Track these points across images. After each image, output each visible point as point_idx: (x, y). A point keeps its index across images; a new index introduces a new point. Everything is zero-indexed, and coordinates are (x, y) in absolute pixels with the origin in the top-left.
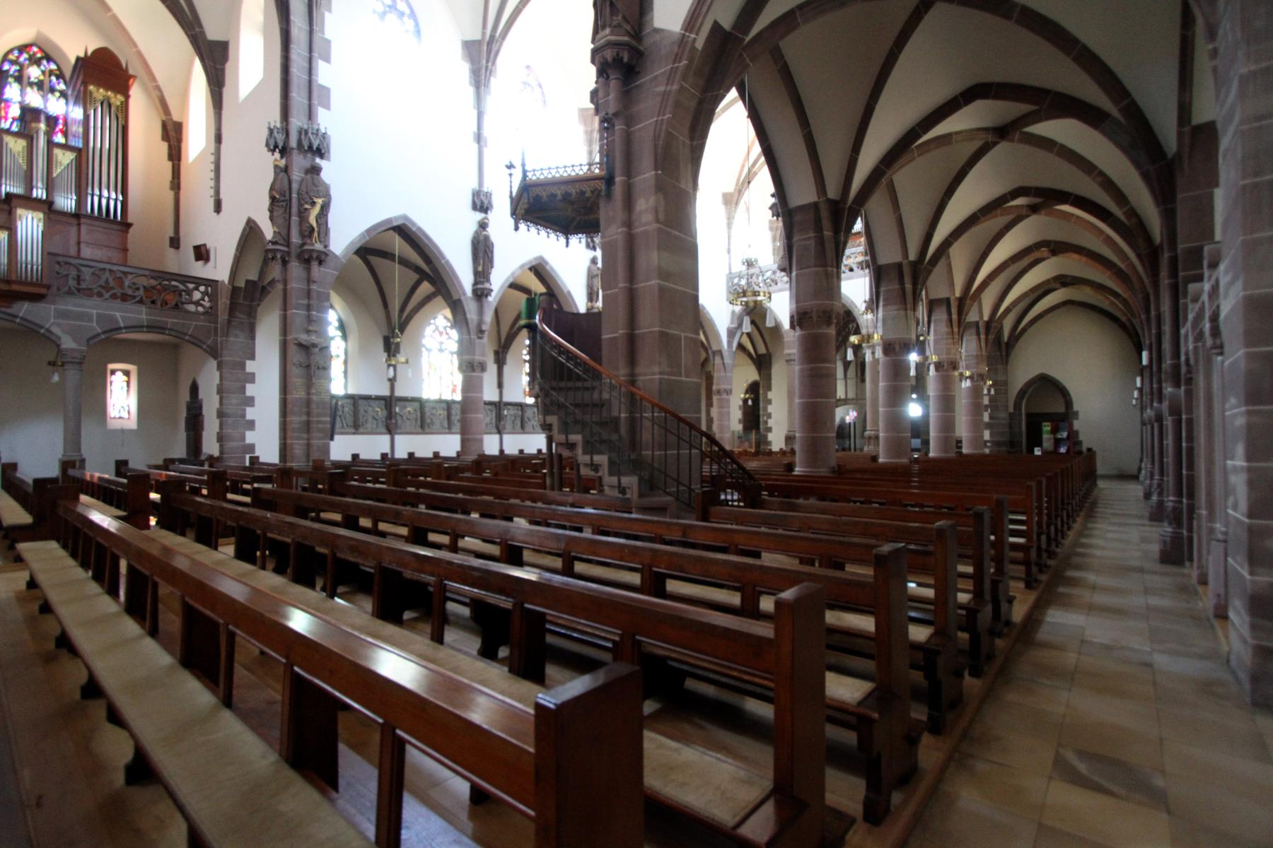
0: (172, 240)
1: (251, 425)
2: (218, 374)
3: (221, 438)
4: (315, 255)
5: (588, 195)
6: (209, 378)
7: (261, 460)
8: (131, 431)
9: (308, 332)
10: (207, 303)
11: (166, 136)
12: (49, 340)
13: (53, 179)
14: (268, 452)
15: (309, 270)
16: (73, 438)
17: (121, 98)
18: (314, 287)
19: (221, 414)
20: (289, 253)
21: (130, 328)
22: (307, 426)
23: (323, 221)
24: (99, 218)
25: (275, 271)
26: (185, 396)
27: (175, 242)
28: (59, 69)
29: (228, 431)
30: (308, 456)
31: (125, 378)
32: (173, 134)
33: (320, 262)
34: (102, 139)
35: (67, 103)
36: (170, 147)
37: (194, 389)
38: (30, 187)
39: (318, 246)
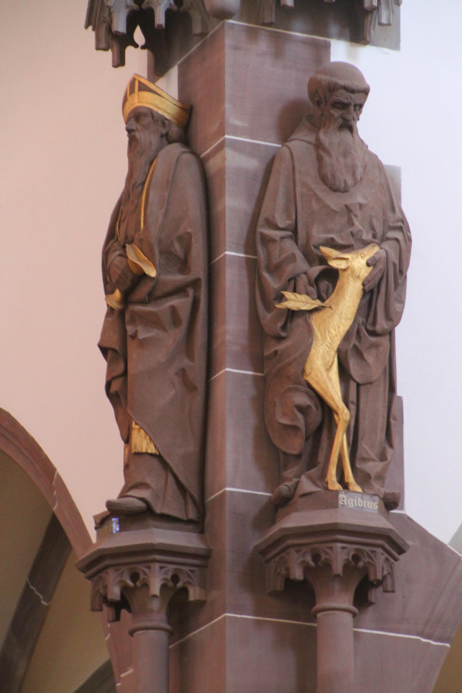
4: (339, 555)
15: (304, 647)
39: (357, 507)
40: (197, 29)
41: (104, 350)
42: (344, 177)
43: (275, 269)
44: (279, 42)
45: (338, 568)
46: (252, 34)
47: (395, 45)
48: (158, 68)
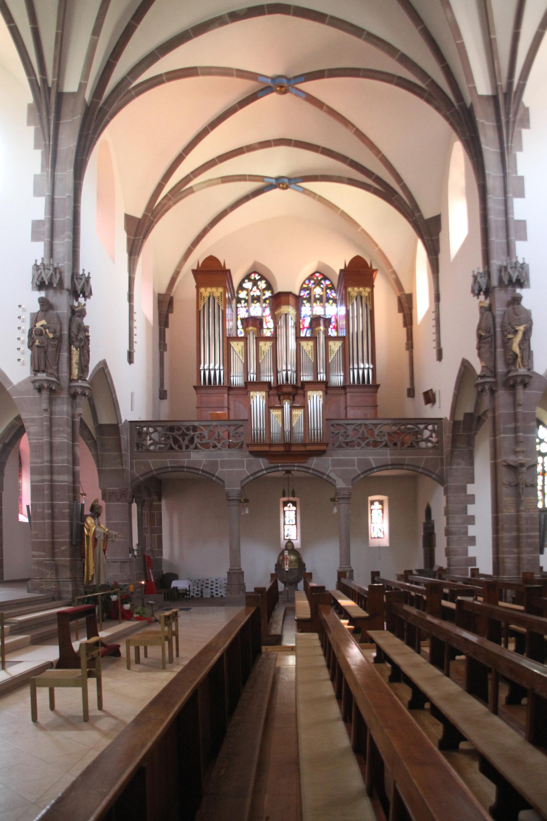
1: (472, 541)
2: (444, 498)
3: (448, 553)
4: (519, 380)
5: (81, 300)
6: (439, 502)
7: (481, 572)
8: (385, 548)
9: (516, 453)
10: (434, 439)
11: (401, 309)
12: (330, 483)
13: (329, 364)
14: (485, 566)
15: (514, 395)
16: (345, 556)
17: (368, 289)
18: (520, 410)
19: (448, 533)
20: (495, 383)
21: (384, 466)
22: (518, 541)
23: (526, 345)
24: (358, 386)
25: (486, 399)
26: (422, 518)
27: (411, 393)
28: (332, 283)
29: (454, 546)
31: (380, 506)
32: (406, 304)
33: (525, 385)
34: (358, 325)
35: (337, 306)
36: (404, 317)
37: (428, 512)
38: (316, 373)
39: (522, 371)
40: (490, 290)
42: (519, 313)
44: (506, 291)
46: (500, 290)
48: (486, 298)
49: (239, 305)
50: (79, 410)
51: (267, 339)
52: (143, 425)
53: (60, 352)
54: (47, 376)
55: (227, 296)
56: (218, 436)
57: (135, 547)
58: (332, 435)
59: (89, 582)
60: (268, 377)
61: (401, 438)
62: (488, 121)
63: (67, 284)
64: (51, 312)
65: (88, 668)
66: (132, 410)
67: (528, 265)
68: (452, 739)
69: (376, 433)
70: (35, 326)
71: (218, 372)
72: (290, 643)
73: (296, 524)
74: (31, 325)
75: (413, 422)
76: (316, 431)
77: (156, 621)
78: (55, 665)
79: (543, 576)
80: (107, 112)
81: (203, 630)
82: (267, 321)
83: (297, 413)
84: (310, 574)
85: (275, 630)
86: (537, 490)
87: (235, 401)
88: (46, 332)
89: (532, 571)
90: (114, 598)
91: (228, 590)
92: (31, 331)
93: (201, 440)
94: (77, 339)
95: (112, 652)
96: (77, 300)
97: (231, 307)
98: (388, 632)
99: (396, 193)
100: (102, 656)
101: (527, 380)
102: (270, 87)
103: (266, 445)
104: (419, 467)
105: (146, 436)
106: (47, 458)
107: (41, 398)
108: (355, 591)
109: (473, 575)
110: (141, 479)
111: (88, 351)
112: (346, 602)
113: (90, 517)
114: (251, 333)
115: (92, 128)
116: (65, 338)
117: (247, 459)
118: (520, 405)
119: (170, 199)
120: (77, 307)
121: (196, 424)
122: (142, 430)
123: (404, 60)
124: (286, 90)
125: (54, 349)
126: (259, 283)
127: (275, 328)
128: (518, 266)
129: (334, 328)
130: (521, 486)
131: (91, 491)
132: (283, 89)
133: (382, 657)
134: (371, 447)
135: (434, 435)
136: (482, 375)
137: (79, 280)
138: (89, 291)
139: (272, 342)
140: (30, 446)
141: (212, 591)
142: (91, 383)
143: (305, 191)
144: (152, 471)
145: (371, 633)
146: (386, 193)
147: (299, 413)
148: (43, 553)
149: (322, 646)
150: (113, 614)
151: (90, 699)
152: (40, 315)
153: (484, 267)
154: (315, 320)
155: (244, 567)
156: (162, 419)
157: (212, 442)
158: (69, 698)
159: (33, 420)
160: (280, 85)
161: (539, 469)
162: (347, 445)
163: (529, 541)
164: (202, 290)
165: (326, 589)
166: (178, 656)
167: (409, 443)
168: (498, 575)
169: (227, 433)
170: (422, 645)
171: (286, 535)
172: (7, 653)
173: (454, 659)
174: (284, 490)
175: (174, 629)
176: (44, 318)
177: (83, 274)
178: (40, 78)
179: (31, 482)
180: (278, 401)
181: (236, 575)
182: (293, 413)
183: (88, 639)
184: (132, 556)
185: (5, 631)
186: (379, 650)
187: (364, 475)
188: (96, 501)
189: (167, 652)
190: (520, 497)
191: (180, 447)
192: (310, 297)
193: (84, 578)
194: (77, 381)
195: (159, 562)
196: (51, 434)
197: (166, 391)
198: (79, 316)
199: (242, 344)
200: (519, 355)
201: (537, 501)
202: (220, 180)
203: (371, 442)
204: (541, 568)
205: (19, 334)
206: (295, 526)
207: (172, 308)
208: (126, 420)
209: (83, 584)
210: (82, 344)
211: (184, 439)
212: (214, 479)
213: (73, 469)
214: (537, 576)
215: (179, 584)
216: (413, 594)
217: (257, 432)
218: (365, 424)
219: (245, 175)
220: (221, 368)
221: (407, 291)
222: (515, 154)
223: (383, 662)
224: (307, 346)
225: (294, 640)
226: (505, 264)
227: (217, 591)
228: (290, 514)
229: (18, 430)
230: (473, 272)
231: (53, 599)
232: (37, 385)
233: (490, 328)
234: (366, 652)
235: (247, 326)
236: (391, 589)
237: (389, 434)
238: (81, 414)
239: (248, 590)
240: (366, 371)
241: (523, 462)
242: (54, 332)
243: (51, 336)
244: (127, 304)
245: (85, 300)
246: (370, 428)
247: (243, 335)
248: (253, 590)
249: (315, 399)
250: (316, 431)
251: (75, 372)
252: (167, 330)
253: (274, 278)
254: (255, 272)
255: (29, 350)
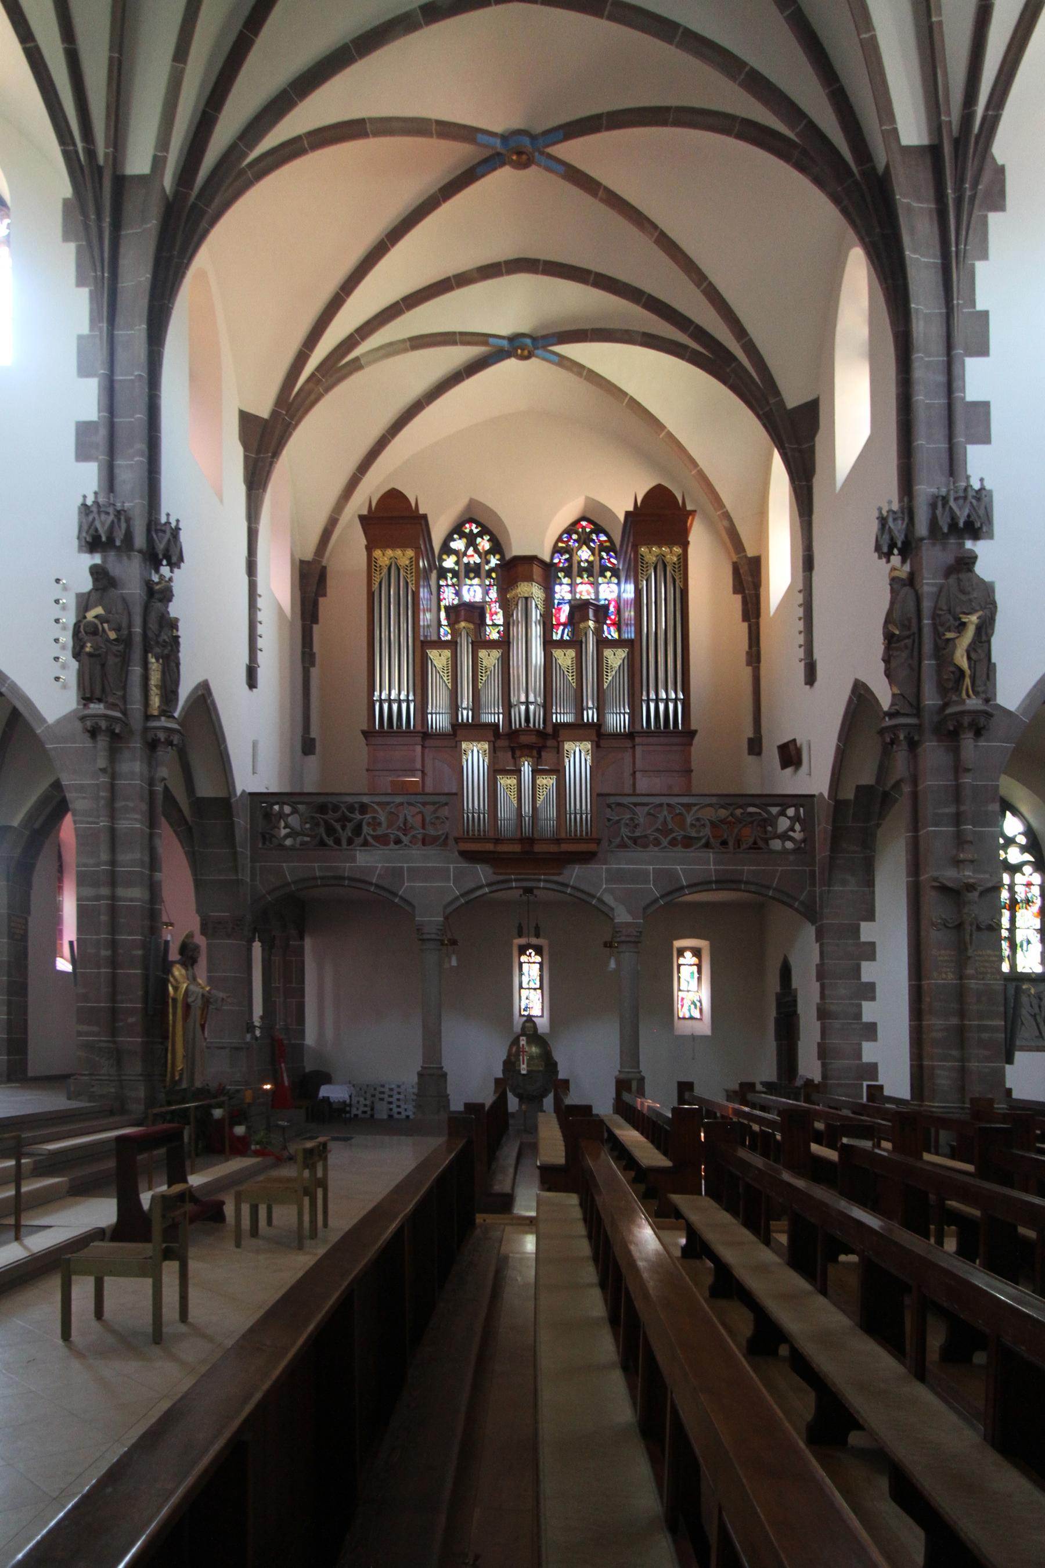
0: (751, 741)
1: (870, 1031)
3: (823, 1052)
4: (966, 720)
5: (165, 570)
6: (806, 954)
7: (887, 1092)
8: (704, 1038)
9: (957, 863)
10: (798, 835)
11: (739, 587)
12: (604, 913)
14: (896, 1082)
15: (956, 751)
16: (630, 1051)
17: (677, 550)
18: (967, 780)
19: (823, 1014)
20: (919, 727)
22: (960, 1036)
26: (773, 985)
27: (755, 746)
28: (610, 540)
30: (962, 1089)
31: (695, 960)
32: (748, 577)
33: (978, 733)
34: (657, 620)
35: (618, 584)
37: (786, 973)
38: (580, 709)
39: (973, 703)
40: (914, 545)
41: (883, 660)
43: (942, 625)
45: (966, 724)
46: (934, 544)
47: (990, 536)
48: (903, 562)
49: (442, 583)
50: (163, 772)
51: (491, 644)
52: (272, 800)
53: (128, 666)
54: (105, 708)
55: (421, 564)
56: (405, 824)
57: (257, 1022)
58: (607, 824)
59: (175, 1083)
60: (492, 716)
61: (736, 831)
62: (919, 200)
63: (140, 541)
64: (114, 593)
65: (164, 1242)
66: (254, 773)
67: (990, 492)
68: (833, 1423)
69: (689, 820)
70: (85, 617)
71: (404, 706)
72: (527, 1210)
73: (541, 988)
74: (77, 615)
75: (757, 801)
76: (578, 816)
77: (291, 1158)
78: (108, 1234)
79: (1011, 1108)
80: (203, 213)
81: (369, 1178)
82: (493, 610)
83: (545, 782)
84: (566, 1083)
85: (502, 1185)
86: (1000, 939)
87: (434, 759)
88: (103, 629)
89: (990, 1096)
90: (218, 1113)
91: (419, 1107)
92: (77, 627)
93: (374, 830)
94: (158, 643)
95: (208, 1212)
96: (157, 571)
97: (429, 586)
98: (708, 1199)
99: (733, 358)
100: (192, 1221)
101: (982, 722)
102: (499, 154)
103: (486, 840)
104: (769, 888)
105: (279, 822)
106: (105, 856)
107: (95, 747)
108: (644, 1115)
109: (871, 1097)
110: (269, 898)
111: (178, 664)
112: (630, 1136)
113: (178, 966)
114: (464, 634)
115: (178, 243)
116: (138, 639)
117: (455, 865)
118: (968, 770)
119: (319, 381)
120: (157, 583)
121: (365, 799)
122: (272, 808)
123: (757, 84)
124: (529, 159)
125: (117, 660)
126: (479, 540)
127: (507, 624)
128: (971, 494)
129: (613, 624)
130: (968, 928)
131: (182, 916)
132: (524, 157)
133: (697, 1248)
134: (679, 848)
135: (797, 827)
136: (893, 711)
137: (160, 534)
138: (178, 553)
139: (500, 651)
140: (77, 836)
141: (391, 1106)
142: (183, 722)
143: (563, 362)
144: (288, 884)
145: (677, 1199)
146: (714, 360)
147: (548, 782)
148: (95, 1029)
149: (585, 1220)
150: (215, 1143)
151: (166, 1299)
152: (92, 598)
153: (901, 500)
154: (579, 609)
155: (448, 1065)
156: (305, 791)
157: (394, 833)
158: (129, 1296)
159: (81, 788)
160: (518, 149)
161: (1005, 895)
162: (635, 843)
163: (985, 1036)
164: (377, 553)
165: (595, 1111)
166: (325, 1224)
167: (751, 841)
168: (922, 1099)
169: (419, 817)
170: (772, 1228)
171: (523, 1007)
172: (25, 1210)
173: (836, 1260)
174: (520, 924)
175: (320, 1174)
176: (100, 602)
177: (168, 523)
178: (84, 148)
179: (78, 900)
180: (511, 760)
181: (433, 1078)
182: (538, 782)
183: (169, 1186)
184: (252, 1038)
185: (23, 1169)
186: (692, 1234)
187: (669, 898)
188: (190, 936)
189: (306, 1218)
190: (966, 949)
191: (338, 842)
192: (571, 566)
193: (165, 1076)
194: (157, 718)
195: (299, 1049)
196: (113, 814)
197: (314, 740)
198: (161, 601)
199: (447, 653)
200: (968, 672)
201: (1001, 959)
202: (408, 344)
203: (679, 838)
204: (1009, 1091)
205: (56, 631)
206: (539, 991)
207: (325, 588)
208: (244, 791)
209: (165, 1087)
210: (166, 652)
211: (344, 828)
212: (396, 900)
213: (151, 877)
214: (1001, 1106)
215: (333, 1092)
216: (756, 1127)
217: (473, 816)
218: (668, 805)
219: (454, 333)
220: (411, 698)
221: (750, 553)
222: (973, 266)
223: (699, 1257)
224: (565, 658)
225: (534, 1204)
226: (943, 491)
227: (399, 1106)
228: (530, 969)
229: (55, 806)
230: (880, 509)
231: (112, 1113)
232: (89, 724)
233: (909, 620)
234: (667, 1235)
235: (457, 622)
236: (715, 1117)
237: (713, 825)
238: (164, 779)
239: (453, 1108)
240: (671, 706)
241: (972, 881)
242: (118, 630)
243: (112, 635)
244: (245, 579)
245: (172, 571)
246: (678, 811)
247: (449, 637)
248: (461, 1108)
249: (578, 757)
250: (578, 816)
251: (156, 701)
252: (315, 627)
253: (505, 531)
254: (471, 521)
255: (74, 660)
